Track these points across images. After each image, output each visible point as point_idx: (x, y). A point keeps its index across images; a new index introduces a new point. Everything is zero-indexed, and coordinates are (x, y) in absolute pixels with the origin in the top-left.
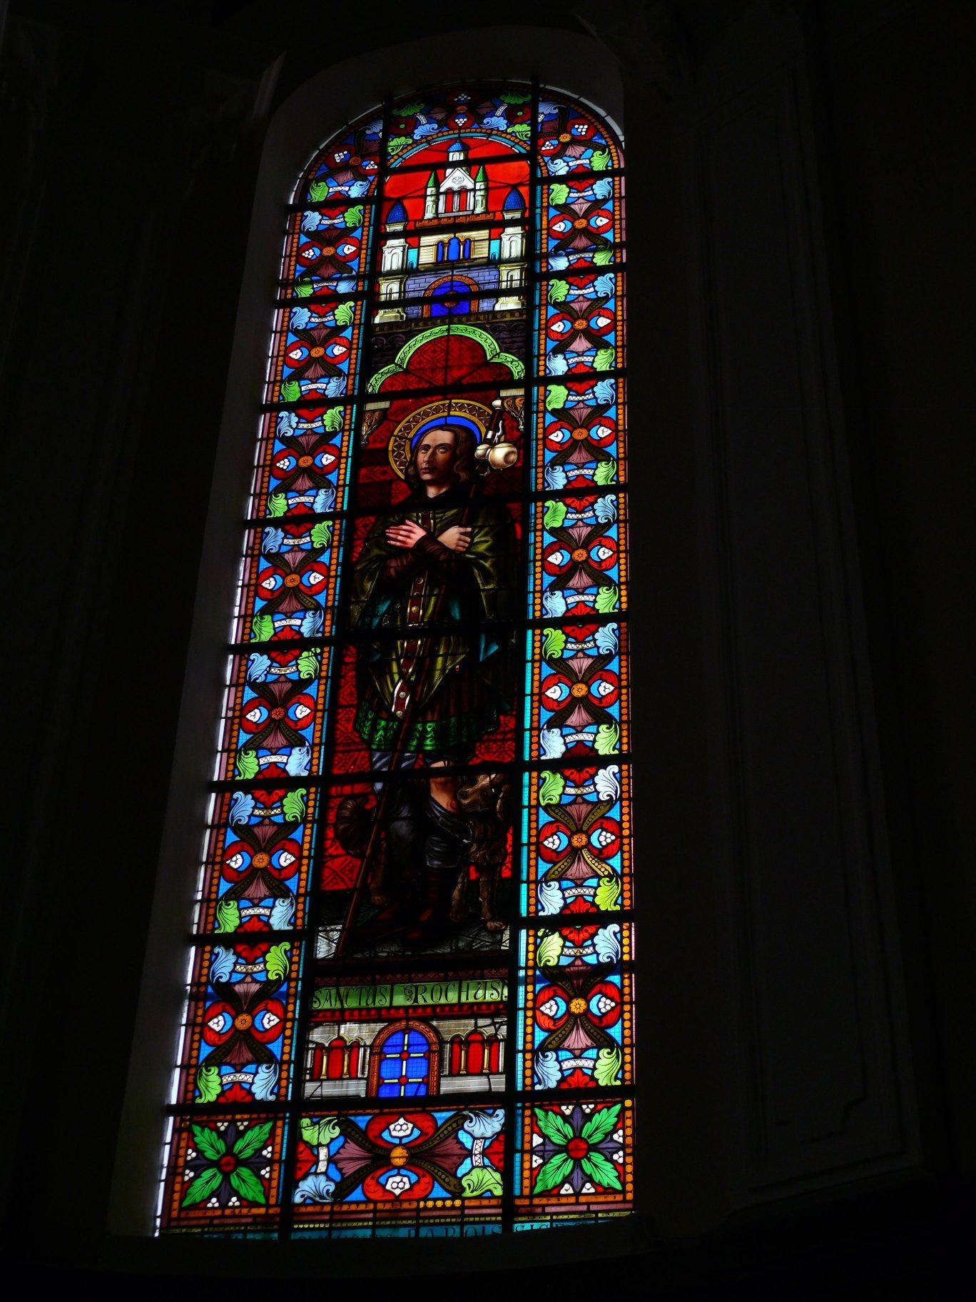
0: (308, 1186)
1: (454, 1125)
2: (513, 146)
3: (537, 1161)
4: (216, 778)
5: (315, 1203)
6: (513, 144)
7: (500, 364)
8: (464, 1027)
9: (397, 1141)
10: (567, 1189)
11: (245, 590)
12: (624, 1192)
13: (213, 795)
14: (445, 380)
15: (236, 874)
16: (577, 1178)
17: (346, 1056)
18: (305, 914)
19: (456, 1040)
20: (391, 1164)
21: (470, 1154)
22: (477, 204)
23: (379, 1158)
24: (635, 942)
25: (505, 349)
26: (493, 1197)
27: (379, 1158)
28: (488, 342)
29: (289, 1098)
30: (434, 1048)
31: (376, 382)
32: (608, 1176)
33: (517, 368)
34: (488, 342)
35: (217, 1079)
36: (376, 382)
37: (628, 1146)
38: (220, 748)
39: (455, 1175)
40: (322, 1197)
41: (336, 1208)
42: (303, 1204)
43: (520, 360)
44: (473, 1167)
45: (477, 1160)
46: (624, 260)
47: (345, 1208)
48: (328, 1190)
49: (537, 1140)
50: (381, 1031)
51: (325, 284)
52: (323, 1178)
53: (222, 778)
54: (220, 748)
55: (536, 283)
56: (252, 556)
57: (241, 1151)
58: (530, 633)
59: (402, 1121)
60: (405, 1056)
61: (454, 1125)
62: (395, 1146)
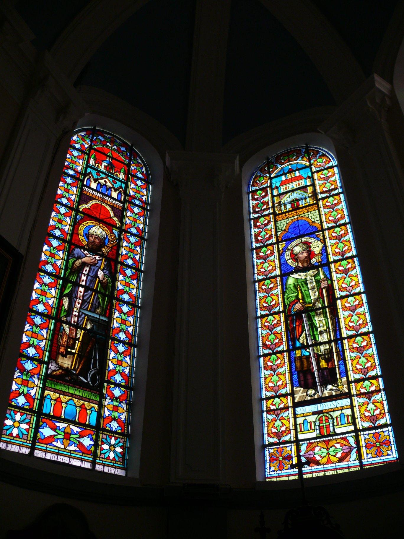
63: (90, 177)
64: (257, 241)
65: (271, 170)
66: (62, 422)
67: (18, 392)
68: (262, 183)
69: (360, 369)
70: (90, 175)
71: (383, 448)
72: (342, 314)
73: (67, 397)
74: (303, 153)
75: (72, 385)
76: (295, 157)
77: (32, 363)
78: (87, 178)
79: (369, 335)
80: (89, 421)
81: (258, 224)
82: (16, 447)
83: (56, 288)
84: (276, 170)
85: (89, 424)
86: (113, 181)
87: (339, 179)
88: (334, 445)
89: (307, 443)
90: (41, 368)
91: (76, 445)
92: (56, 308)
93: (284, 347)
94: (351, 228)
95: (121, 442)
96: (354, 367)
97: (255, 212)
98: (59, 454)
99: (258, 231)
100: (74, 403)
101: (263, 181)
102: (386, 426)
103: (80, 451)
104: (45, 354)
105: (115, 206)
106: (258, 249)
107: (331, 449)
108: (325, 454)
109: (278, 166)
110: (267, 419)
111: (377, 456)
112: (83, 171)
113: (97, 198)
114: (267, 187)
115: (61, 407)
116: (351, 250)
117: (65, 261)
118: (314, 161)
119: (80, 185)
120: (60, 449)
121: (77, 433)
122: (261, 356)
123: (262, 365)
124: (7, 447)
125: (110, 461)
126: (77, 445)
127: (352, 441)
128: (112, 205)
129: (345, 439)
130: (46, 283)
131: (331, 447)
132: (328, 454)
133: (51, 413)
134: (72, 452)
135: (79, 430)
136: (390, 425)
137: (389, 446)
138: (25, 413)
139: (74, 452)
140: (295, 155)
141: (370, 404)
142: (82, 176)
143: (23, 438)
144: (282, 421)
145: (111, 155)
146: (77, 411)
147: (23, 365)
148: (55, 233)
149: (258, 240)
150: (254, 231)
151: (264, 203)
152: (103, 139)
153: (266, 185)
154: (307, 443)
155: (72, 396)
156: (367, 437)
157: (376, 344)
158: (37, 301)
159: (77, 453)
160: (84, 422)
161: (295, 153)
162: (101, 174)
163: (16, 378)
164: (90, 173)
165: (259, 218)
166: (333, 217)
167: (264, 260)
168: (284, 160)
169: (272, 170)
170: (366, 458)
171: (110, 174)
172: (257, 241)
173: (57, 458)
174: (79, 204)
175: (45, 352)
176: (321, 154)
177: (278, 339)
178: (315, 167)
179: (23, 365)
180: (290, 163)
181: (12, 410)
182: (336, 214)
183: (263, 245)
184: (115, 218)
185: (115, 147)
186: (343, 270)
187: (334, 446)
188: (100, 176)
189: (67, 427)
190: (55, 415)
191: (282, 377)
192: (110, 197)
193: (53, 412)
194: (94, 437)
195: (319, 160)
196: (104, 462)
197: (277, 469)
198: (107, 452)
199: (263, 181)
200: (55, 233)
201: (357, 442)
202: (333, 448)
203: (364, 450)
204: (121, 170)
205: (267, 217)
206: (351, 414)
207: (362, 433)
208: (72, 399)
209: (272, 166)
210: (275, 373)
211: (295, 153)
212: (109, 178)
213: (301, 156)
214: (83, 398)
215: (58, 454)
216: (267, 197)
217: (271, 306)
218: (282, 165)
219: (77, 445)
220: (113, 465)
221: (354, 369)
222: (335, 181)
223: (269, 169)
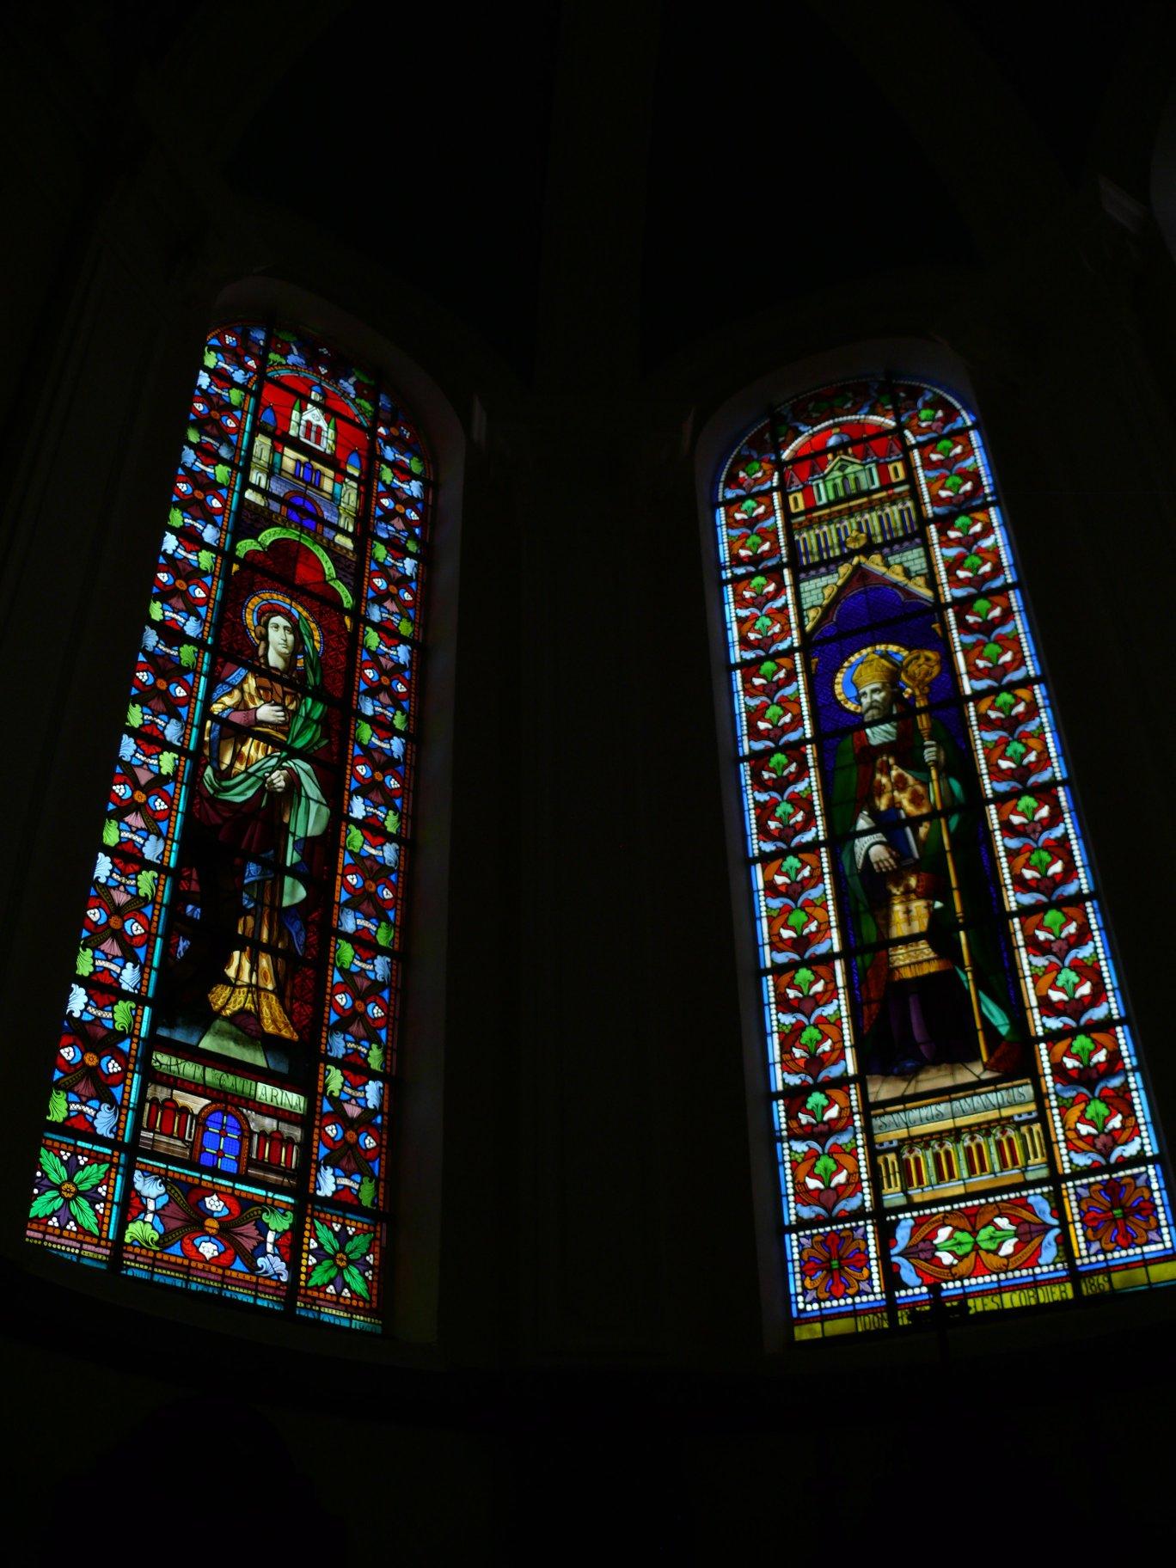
0: (135, 1230)
1: (166, 1240)
3: (102, 1190)
5: (142, 1247)
8: (269, 1124)
9: (213, 1239)
10: (331, 1289)
12: (371, 1302)
15: (93, 926)
16: (339, 1281)
17: (177, 1118)
19: (263, 1135)
20: (219, 1222)
21: (155, 1213)
22: (327, 444)
23: (196, 1220)
26: (142, 1171)
27: (196, 1220)
28: (328, 567)
30: (246, 1134)
32: (358, 1285)
33: (347, 600)
34: (328, 567)
35: (65, 1105)
37: (306, 1251)
39: (170, 1197)
40: (147, 1243)
41: (159, 1256)
42: (131, 1244)
44: (154, 1199)
45: (151, 1206)
47: (166, 1258)
48: (152, 1239)
49: (314, 1245)
50: (206, 1106)
51: (211, 441)
52: (149, 1226)
57: (349, 1272)
59: (215, 1197)
60: (223, 1134)
61: (166, 1240)
62: (214, 1237)
64: (755, 734)
65: (781, 439)
68: (756, 480)
69: (1089, 1135)
71: (1130, 1199)
72: (981, 739)
74: (874, 394)
76: (849, 405)
79: (1111, 1031)
81: (747, 594)
84: (797, 442)
87: (1006, 542)
88: (992, 1221)
89: (912, 1218)
92: (166, 906)
93: (819, 831)
94: (992, 475)
96: (1069, 1129)
97: (737, 561)
99: (794, 1021)
101: (759, 475)
102: (1140, 1159)
106: (795, 1098)
107: (984, 1234)
108: (968, 1248)
109: (802, 428)
110: (793, 1154)
111: (1118, 1245)
112: (173, 855)
114: (772, 489)
116: (1023, 663)
117: (164, 909)
118: (911, 418)
122: (754, 861)
123: (770, 995)
127: (1043, 1208)
129: (1024, 1204)
131: (985, 1226)
132: (976, 1247)
136: (1153, 1160)
137: (1151, 1217)
140: (850, 399)
141: (1092, 1103)
142: (188, 762)
144: (807, 909)
149: (744, 599)
150: (776, 1020)
151: (785, 704)
153: (767, 486)
154: (912, 1218)
156: (1084, 1193)
157: (1004, 524)
161: (850, 395)
165: (759, 661)
166: (1062, 989)
167: (768, 696)
168: (817, 412)
169: (784, 441)
170: (1084, 1253)
172: (764, 833)
176: (928, 396)
177: (845, 1172)
178: (914, 434)
180: (836, 420)
182: (1021, 749)
183: (771, 745)
186: (959, 538)
187: (991, 1223)
191: (818, 912)
195: (924, 414)
197: (827, 1295)
199: (759, 475)
201: (1059, 1210)
202: (991, 1229)
203: (1077, 1233)
205: (782, 661)
206: (925, 571)
207: (1070, 1184)
209: (783, 429)
210: (796, 902)
211: (850, 395)
213: (869, 403)
216: (807, 780)
217: (798, 882)
218: (813, 425)
221: (1071, 1135)
222: (995, 551)
223: (775, 436)
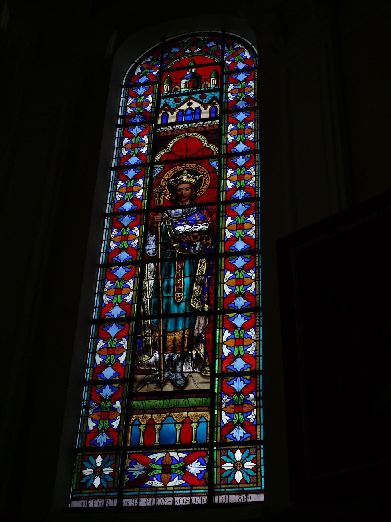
2: (214, 59)
4: (107, 212)
6: (214, 58)
7: (209, 148)
11: (117, 159)
13: (100, 269)
14: (187, 155)
18: (127, 391)
24: (260, 194)
25: (209, 142)
29: (135, 316)
31: (158, 158)
34: (203, 139)
36: (158, 158)
38: (114, 157)
43: (216, 146)
46: (259, 149)
53: (110, 212)
54: (114, 157)
55: (219, 258)
56: (125, 97)
58: (223, 159)
63: (166, 110)
66: (158, 451)
67: (232, 424)
70: (166, 108)
73: (163, 415)
75: (195, 395)
77: (242, 379)
78: (160, 115)
80: (196, 439)
82: (224, 497)
83: (135, 277)
85: (197, 442)
86: (200, 97)
90: (256, 381)
91: (180, 477)
95: (226, 453)
98: (189, 494)
100: (174, 420)
103: (187, 484)
104: (258, 361)
105: (207, 129)
113: (179, 132)
115: (191, 428)
119: (257, 114)
120: (159, 489)
121: (182, 460)
124: (88, 503)
125: (237, 486)
126: (182, 476)
128: (202, 129)
130: (240, 268)
133: (178, 442)
134: (176, 488)
135: (183, 455)
138: (246, 448)
139: (179, 488)
143: (251, 482)
145: (193, 64)
146: (177, 429)
147: (232, 386)
148: (237, 196)
152: (178, 50)
155: (157, 411)
158: (233, 295)
159: (183, 488)
160: (173, 442)
162: (207, 94)
163: (93, 414)
164: (166, 104)
171: (195, 90)
173: (191, 500)
174: (154, 154)
175: (258, 358)
179: (232, 386)
181: (228, 449)
184: (210, 146)
185: (198, 49)
188: (180, 100)
189: (165, 456)
190: (162, 444)
192: (200, 120)
193: (180, 440)
194: (207, 459)
196: (227, 490)
198: (246, 472)
200: (124, 208)
204: (211, 75)
208: (170, 416)
212: (195, 96)
214: (147, 410)
215: (156, 496)
219: (182, 476)
220: (225, 491)
